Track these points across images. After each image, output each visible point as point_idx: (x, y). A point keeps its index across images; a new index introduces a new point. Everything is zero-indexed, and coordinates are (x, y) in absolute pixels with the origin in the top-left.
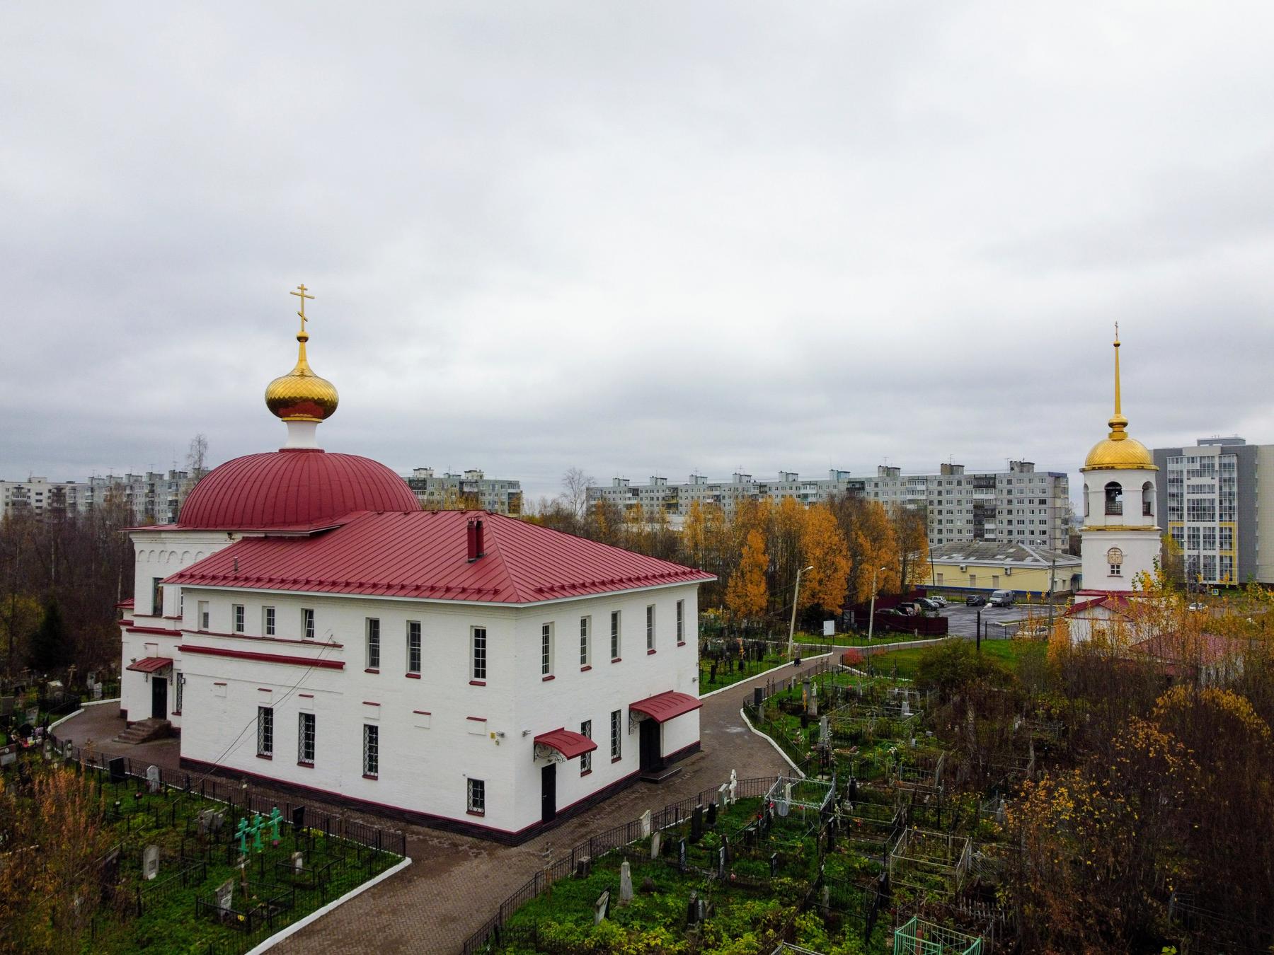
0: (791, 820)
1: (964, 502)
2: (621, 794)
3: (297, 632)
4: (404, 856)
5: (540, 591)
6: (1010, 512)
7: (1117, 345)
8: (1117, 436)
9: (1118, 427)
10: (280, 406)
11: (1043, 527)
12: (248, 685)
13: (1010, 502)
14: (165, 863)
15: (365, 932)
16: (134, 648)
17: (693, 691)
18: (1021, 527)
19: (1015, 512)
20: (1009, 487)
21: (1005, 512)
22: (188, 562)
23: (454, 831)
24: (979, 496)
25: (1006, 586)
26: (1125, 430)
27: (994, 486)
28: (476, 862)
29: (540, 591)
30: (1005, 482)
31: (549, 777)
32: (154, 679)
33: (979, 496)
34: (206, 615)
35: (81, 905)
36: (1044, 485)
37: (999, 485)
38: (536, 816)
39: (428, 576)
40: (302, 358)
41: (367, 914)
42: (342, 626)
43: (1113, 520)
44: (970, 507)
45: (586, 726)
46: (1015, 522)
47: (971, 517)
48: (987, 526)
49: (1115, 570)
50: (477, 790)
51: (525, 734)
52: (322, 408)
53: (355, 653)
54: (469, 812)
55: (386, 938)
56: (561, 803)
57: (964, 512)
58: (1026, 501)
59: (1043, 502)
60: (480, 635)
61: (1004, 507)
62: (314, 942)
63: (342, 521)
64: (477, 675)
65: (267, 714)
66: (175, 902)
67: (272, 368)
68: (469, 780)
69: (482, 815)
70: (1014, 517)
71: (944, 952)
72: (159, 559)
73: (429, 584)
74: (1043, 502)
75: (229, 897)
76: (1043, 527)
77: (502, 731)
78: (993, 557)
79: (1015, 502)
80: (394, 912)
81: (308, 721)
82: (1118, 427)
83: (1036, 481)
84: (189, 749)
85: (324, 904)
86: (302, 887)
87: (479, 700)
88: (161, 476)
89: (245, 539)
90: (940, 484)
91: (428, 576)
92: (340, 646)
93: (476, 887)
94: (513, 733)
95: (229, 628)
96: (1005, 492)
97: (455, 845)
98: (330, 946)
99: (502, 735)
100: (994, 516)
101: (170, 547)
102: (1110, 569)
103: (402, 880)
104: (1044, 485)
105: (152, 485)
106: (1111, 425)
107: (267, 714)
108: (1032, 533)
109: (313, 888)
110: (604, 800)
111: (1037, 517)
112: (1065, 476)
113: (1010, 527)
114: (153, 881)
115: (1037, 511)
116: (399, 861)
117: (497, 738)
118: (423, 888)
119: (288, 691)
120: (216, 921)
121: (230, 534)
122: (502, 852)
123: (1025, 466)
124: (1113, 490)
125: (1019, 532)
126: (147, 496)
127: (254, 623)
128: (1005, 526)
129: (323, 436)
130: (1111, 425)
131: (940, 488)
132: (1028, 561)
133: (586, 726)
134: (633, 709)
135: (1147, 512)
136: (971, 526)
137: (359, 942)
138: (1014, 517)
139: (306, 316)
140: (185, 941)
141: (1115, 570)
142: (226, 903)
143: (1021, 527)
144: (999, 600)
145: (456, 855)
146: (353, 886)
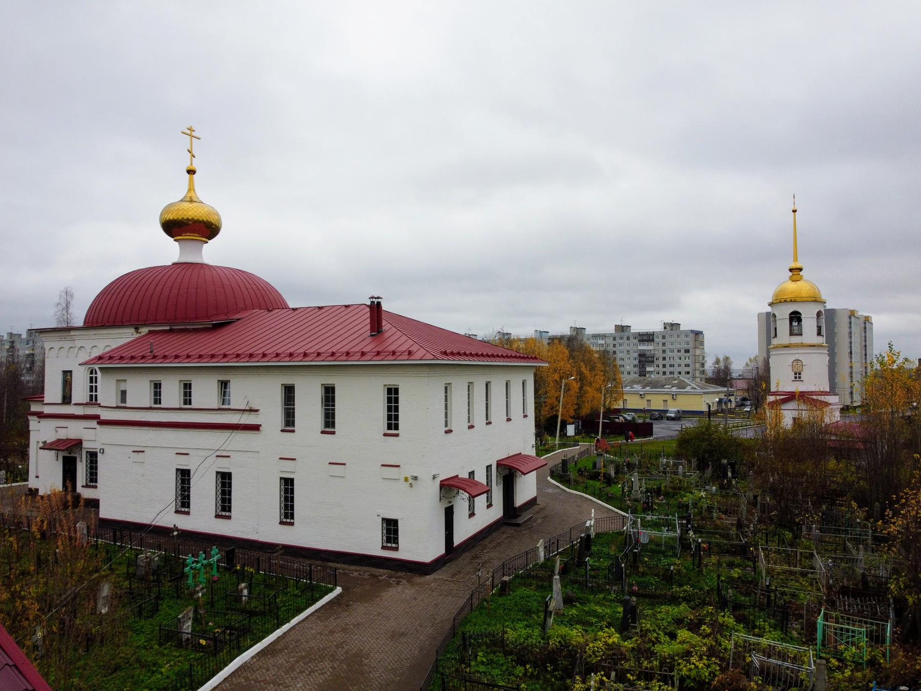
0: (653, 547)
1: (631, 352)
2: (494, 535)
3: (213, 401)
4: (336, 585)
5: (445, 353)
6: (664, 359)
7: (794, 211)
8: (795, 277)
9: (796, 271)
10: (174, 227)
11: (687, 369)
12: (165, 451)
13: (664, 351)
14: (116, 599)
15: (325, 649)
16: (41, 432)
17: (533, 453)
18: (672, 369)
19: (667, 359)
20: (664, 341)
21: (661, 359)
22: (96, 353)
23: (368, 565)
24: (642, 347)
25: (673, 408)
26: (801, 273)
27: (653, 340)
28: (399, 588)
29: (445, 353)
30: (661, 337)
31: (449, 513)
32: (64, 458)
33: (642, 347)
34: (124, 393)
35: (44, 637)
36: (688, 339)
37: (656, 340)
38: (442, 551)
39: (344, 343)
40: (191, 188)
41: (321, 634)
42: (258, 394)
43: (796, 340)
44: (636, 355)
45: (472, 474)
46: (668, 366)
47: (637, 362)
48: (648, 369)
49: (798, 376)
50: (391, 528)
51: (434, 477)
52: (208, 229)
53: (271, 414)
54: (383, 548)
55: (346, 653)
56: (458, 540)
57: (632, 359)
58: (676, 351)
59: (687, 351)
60: (393, 394)
61: (659, 354)
62: (281, 660)
63: (236, 317)
64: (389, 427)
65: (184, 476)
66: (134, 631)
67: (170, 194)
68: (383, 519)
69: (396, 549)
70: (667, 362)
71: (542, 688)
72: (58, 360)
73: (345, 349)
74: (687, 351)
75: (190, 623)
76: (687, 369)
77: (415, 475)
78: (663, 386)
79: (668, 351)
80: (344, 630)
81: (225, 479)
82: (796, 271)
83: (683, 336)
84: (105, 512)
85: (278, 626)
86: (252, 613)
87: (392, 449)
88: (20, 335)
89: (150, 332)
90: (614, 339)
91: (344, 343)
92: (257, 411)
93: (439, 603)
94: (425, 477)
95: (147, 401)
96: (661, 344)
97: (373, 576)
98: (297, 662)
99: (415, 478)
100: (653, 362)
101: (78, 343)
102: (794, 376)
103: (339, 605)
104: (688, 339)
105: (13, 342)
106: (791, 270)
107: (184, 476)
108: (680, 373)
109: (263, 614)
110: (483, 539)
111: (683, 362)
112: (702, 333)
113: (664, 370)
114: (107, 614)
115: (683, 358)
116: (331, 590)
117: (410, 481)
118: (360, 611)
119: (203, 454)
120: (180, 645)
121: (137, 329)
122: (418, 579)
123: (674, 326)
124: (795, 317)
125: (671, 373)
126: (8, 350)
127: (172, 394)
128: (661, 369)
129: (211, 253)
130: (791, 270)
131: (614, 342)
132: (688, 389)
133: (472, 474)
134: (500, 464)
135: (819, 334)
136: (637, 369)
137: (322, 658)
138: (667, 362)
139: (194, 152)
140: (154, 665)
141: (798, 376)
142: (188, 626)
143: (672, 369)
144: (673, 415)
145: (379, 586)
146: (299, 611)
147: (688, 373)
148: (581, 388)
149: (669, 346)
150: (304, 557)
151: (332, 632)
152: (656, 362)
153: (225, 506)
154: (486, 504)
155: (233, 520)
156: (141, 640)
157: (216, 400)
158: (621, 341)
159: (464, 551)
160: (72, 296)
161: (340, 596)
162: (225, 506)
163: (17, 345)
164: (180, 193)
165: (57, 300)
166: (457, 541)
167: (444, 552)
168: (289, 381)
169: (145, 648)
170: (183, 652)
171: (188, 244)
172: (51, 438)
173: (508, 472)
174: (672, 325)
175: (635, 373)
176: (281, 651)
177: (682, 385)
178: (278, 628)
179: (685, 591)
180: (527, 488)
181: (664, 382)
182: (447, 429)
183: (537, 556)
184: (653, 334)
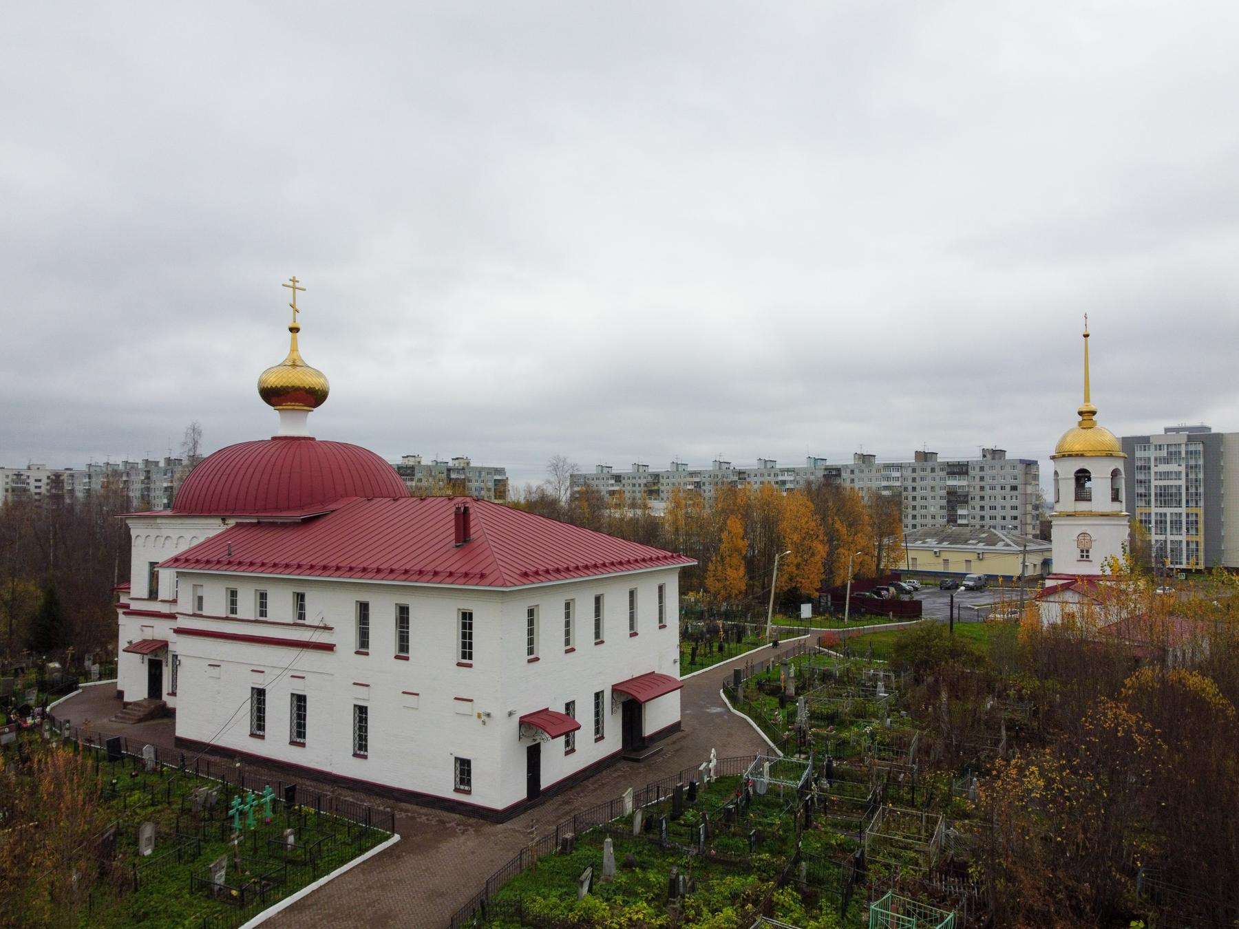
0: (769, 797)
1: (937, 489)
3: (289, 615)
4: (393, 833)
5: (525, 575)
6: (982, 498)
7: (1086, 336)
8: (1087, 424)
9: (1087, 415)
10: (272, 395)
11: (1014, 513)
12: (241, 666)
13: (982, 488)
14: (160, 840)
16: (130, 630)
18: (993, 513)
19: (987, 498)
20: (982, 474)
21: (978, 498)
22: (183, 547)
25: (978, 570)
26: (1094, 418)
27: (967, 473)
28: (462, 839)
29: (525, 575)
30: (977, 469)
31: (534, 756)
32: (150, 660)
34: (200, 599)
35: (79, 880)
37: (971, 472)
38: (522, 794)
40: (294, 348)
41: (357, 889)
42: (332, 609)
43: (1083, 506)
44: (944, 493)
45: (570, 706)
46: (987, 508)
47: (944, 502)
48: (960, 512)
49: (1085, 555)
50: (464, 769)
51: (510, 714)
52: (313, 397)
53: (345, 636)
54: (456, 790)
55: (375, 913)
56: (546, 781)
57: (938, 498)
58: (998, 488)
59: (1014, 488)
60: (467, 617)
61: (976, 493)
62: (306, 917)
65: (259, 695)
68: (456, 759)
69: (469, 792)
70: (986, 503)
71: (918, 926)
73: (417, 568)
74: (1014, 488)
75: (223, 872)
76: (1014, 513)
78: (966, 542)
79: (987, 488)
80: (383, 887)
81: (300, 702)
82: (1087, 415)
83: (1008, 468)
84: (183, 729)
85: (315, 879)
87: (466, 681)
89: (238, 524)
90: (914, 470)
92: (331, 629)
93: (463, 863)
94: (498, 712)
95: (223, 611)
96: (977, 478)
97: (442, 822)
98: (321, 920)
99: (488, 715)
100: (967, 502)
101: (165, 532)
106: (1081, 413)
107: (259, 695)
108: (1004, 518)
110: (587, 778)
111: (1008, 503)
112: (1035, 463)
113: (983, 513)
114: (149, 857)
115: (1008, 498)
117: (484, 718)
118: (411, 864)
119: (280, 673)
121: (223, 520)
122: (489, 829)
123: (997, 454)
124: (1082, 477)
126: (143, 482)
127: (247, 606)
128: (977, 512)
129: (315, 425)
130: (1081, 413)
131: (914, 475)
132: (1000, 546)
133: (570, 706)
134: (616, 689)
135: (1115, 498)
136: (944, 512)
138: (986, 503)
139: (297, 307)
140: (179, 916)
141: (1085, 555)
142: (220, 878)
143: (993, 513)
144: (971, 583)
145: (443, 832)
146: (343, 862)
149: (988, 482)
151: (370, 888)
152: (971, 503)
154: (594, 737)
156: (172, 888)
157: (291, 612)
160: (200, 434)
161: (396, 845)
163: (154, 477)
164: (283, 355)
168: (363, 597)
169: (176, 897)
171: (289, 414)
172: (137, 639)
174: (994, 452)
175: (943, 517)
179: (761, 860)
181: (968, 536)
182: (532, 657)
184: (967, 465)
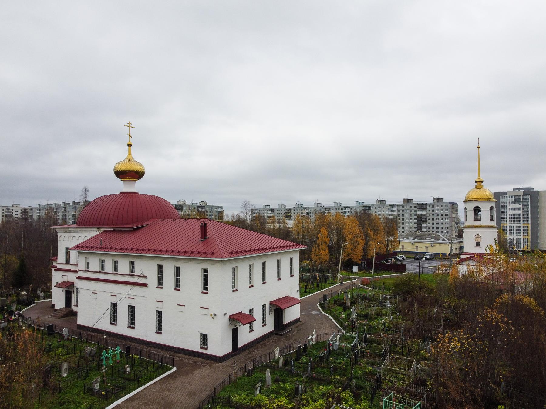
0: (339, 351)
1: (413, 215)
2: (266, 340)
5: (232, 253)
6: (433, 219)
7: (479, 148)
9: (479, 183)
10: (120, 174)
11: (447, 226)
13: (433, 215)
16: (57, 277)
18: (438, 226)
19: (435, 219)
21: (431, 219)
22: (81, 241)
25: (431, 251)
26: (482, 184)
27: (426, 208)
29: (232, 253)
30: (431, 206)
31: (235, 333)
32: (66, 291)
34: (88, 264)
35: (35, 388)
36: (448, 208)
37: (428, 208)
38: (230, 349)
39: (183, 247)
40: (130, 153)
41: (157, 392)
42: (146, 268)
43: (477, 223)
44: (416, 217)
45: (251, 311)
46: (435, 224)
47: (416, 221)
48: (423, 225)
49: (478, 244)
50: (204, 338)
51: (225, 314)
52: (138, 175)
53: (152, 280)
54: (201, 348)
55: (165, 402)
58: (440, 215)
59: (447, 215)
60: (206, 272)
61: (430, 217)
62: (135, 404)
63: (147, 223)
65: (114, 306)
66: (75, 386)
69: (207, 349)
70: (434, 221)
71: (404, 408)
73: (184, 250)
74: (447, 215)
75: (98, 384)
76: (447, 226)
78: (425, 239)
81: (132, 309)
82: (479, 183)
83: (444, 206)
84: (81, 321)
85: (139, 387)
86: (129, 380)
87: (205, 300)
88: (69, 204)
90: (403, 207)
92: (146, 277)
94: (220, 314)
95: (98, 269)
96: (431, 211)
97: (195, 362)
99: (215, 315)
100: (426, 221)
101: (73, 234)
102: (476, 244)
104: (448, 208)
105: (65, 208)
106: (476, 182)
107: (114, 306)
108: (442, 228)
110: (259, 343)
111: (444, 221)
113: (433, 226)
114: (66, 377)
115: (444, 219)
117: (213, 316)
118: (181, 380)
119: (123, 296)
120: (93, 394)
121: (99, 229)
122: (215, 365)
123: (439, 200)
124: (477, 210)
127: (109, 267)
128: (431, 225)
129: (139, 187)
130: (476, 182)
132: (441, 240)
133: (251, 311)
134: (271, 303)
135: (492, 219)
136: (416, 225)
138: (434, 221)
140: (79, 403)
141: (478, 244)
142: (97, 386)
143: (438, 226)
144: (428, 257)
145: (195, 366)
146: (151, 379)
147: (447, 228)
148: (366, 244)
150: (166, 350)
151: (163, 391)
152: (428, 221)
153: (132, 323)
155: (135, 330)
156: (76, 391)
158: (406, 209)
159: (245, 350)
161: (174, 372)
162: (132, 323)
163: (68, 210)
164: (125, 156)
165: (81, 193)
166: (240, 345)
167: (231, 350)
168: (160, 263)
169: (78, 395)
170: (93, 398)
171: (127, 182)
173: (278, 308)
174: (438, 199)
175: (415, 228)
176: (137, 399)
177: (437, 238)
178: (139, 388)
180: (292, 313)
181: (427, 236)
183: (274, 356)
184: (426, 205)
